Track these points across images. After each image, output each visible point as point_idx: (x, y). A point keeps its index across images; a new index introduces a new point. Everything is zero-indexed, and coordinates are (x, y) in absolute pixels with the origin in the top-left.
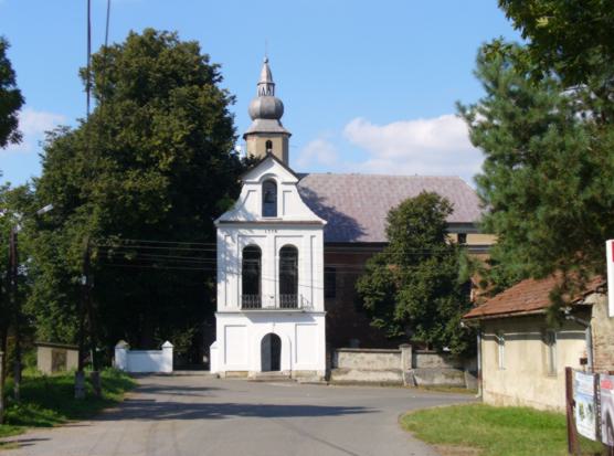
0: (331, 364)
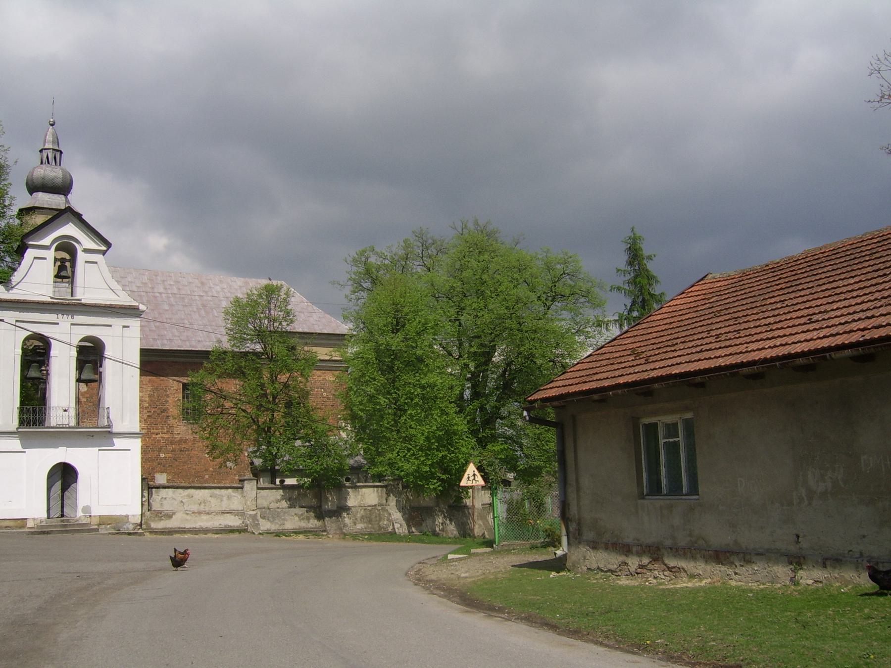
0: (147, 504)
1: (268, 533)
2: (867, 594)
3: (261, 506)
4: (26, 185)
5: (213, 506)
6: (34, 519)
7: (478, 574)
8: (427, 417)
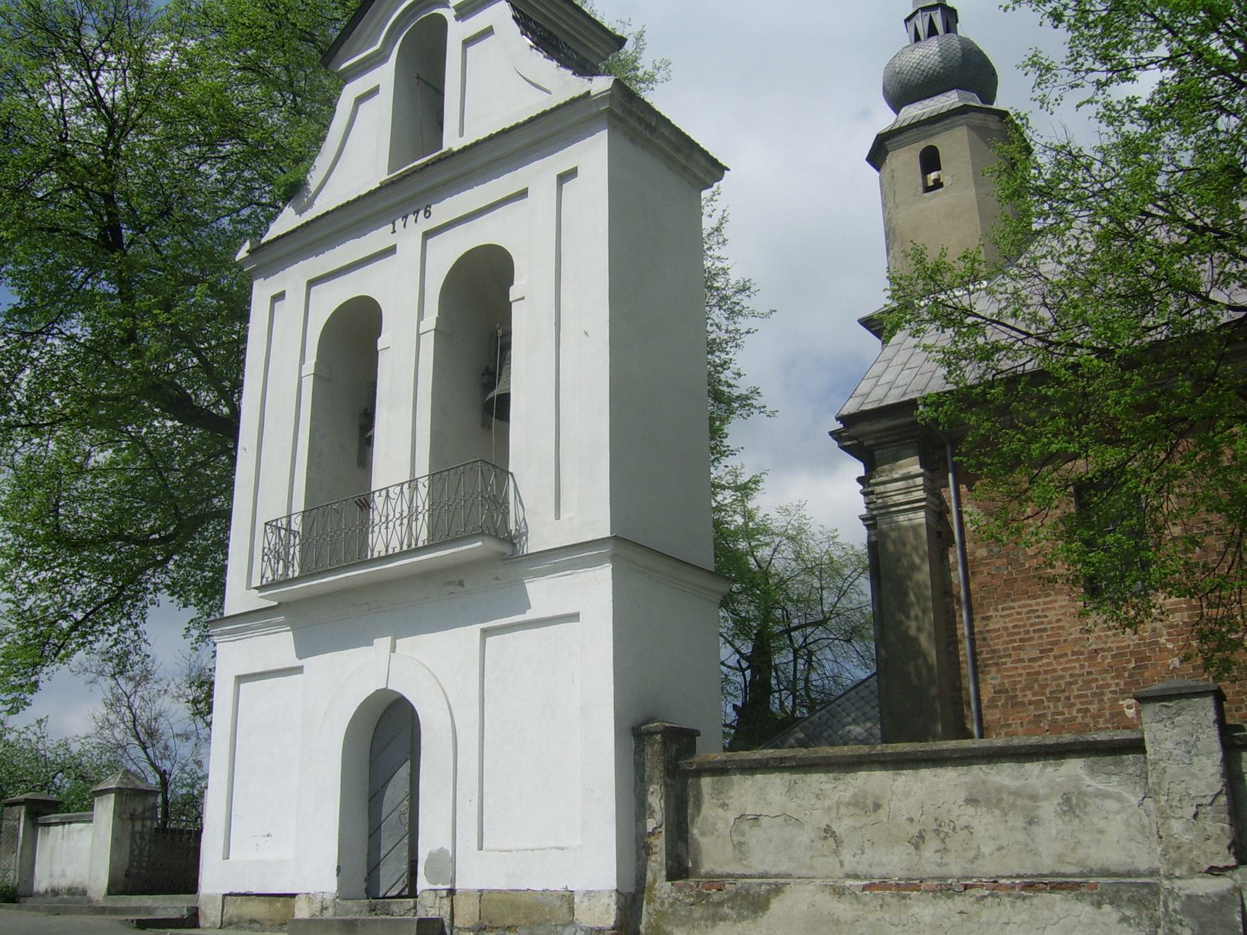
2: (884, 885)
5: (986, 850)
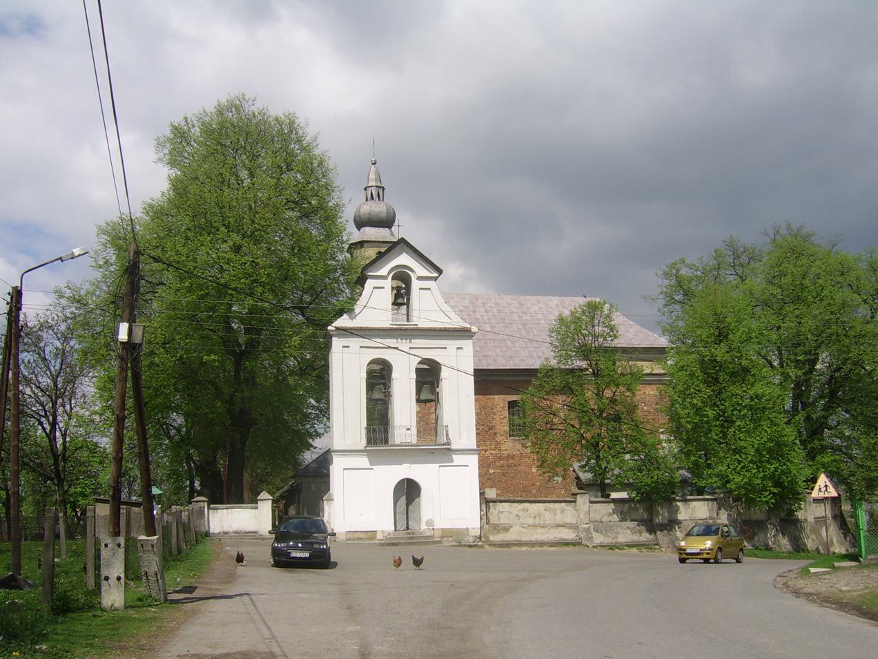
0: (485, 518)
1: (601, 546)
3: (593, 520)
4: (354, 221)
6: (383, 531)
7: (860, 588)
8: (756, 428)
